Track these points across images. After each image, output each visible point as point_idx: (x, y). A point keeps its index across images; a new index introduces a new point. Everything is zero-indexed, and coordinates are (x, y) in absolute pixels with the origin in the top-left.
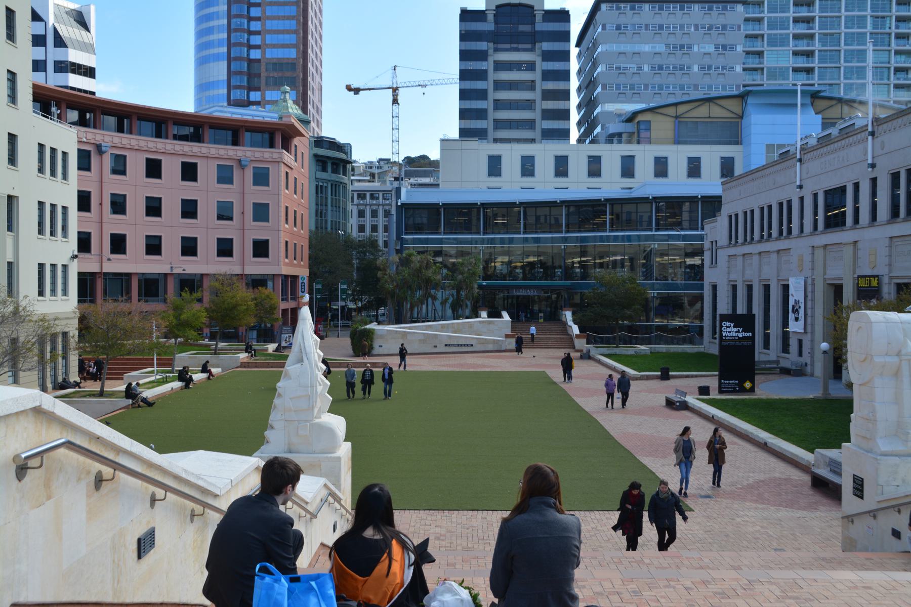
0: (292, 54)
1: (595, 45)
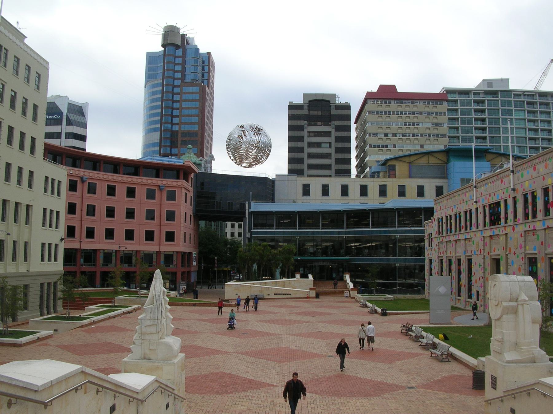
0: (196, 128)
1: (365, 122)
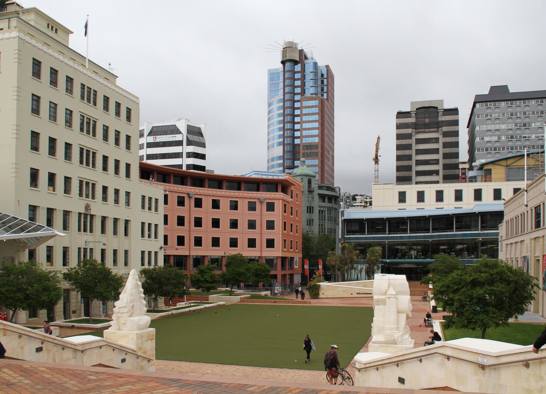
0: (316, 140)
